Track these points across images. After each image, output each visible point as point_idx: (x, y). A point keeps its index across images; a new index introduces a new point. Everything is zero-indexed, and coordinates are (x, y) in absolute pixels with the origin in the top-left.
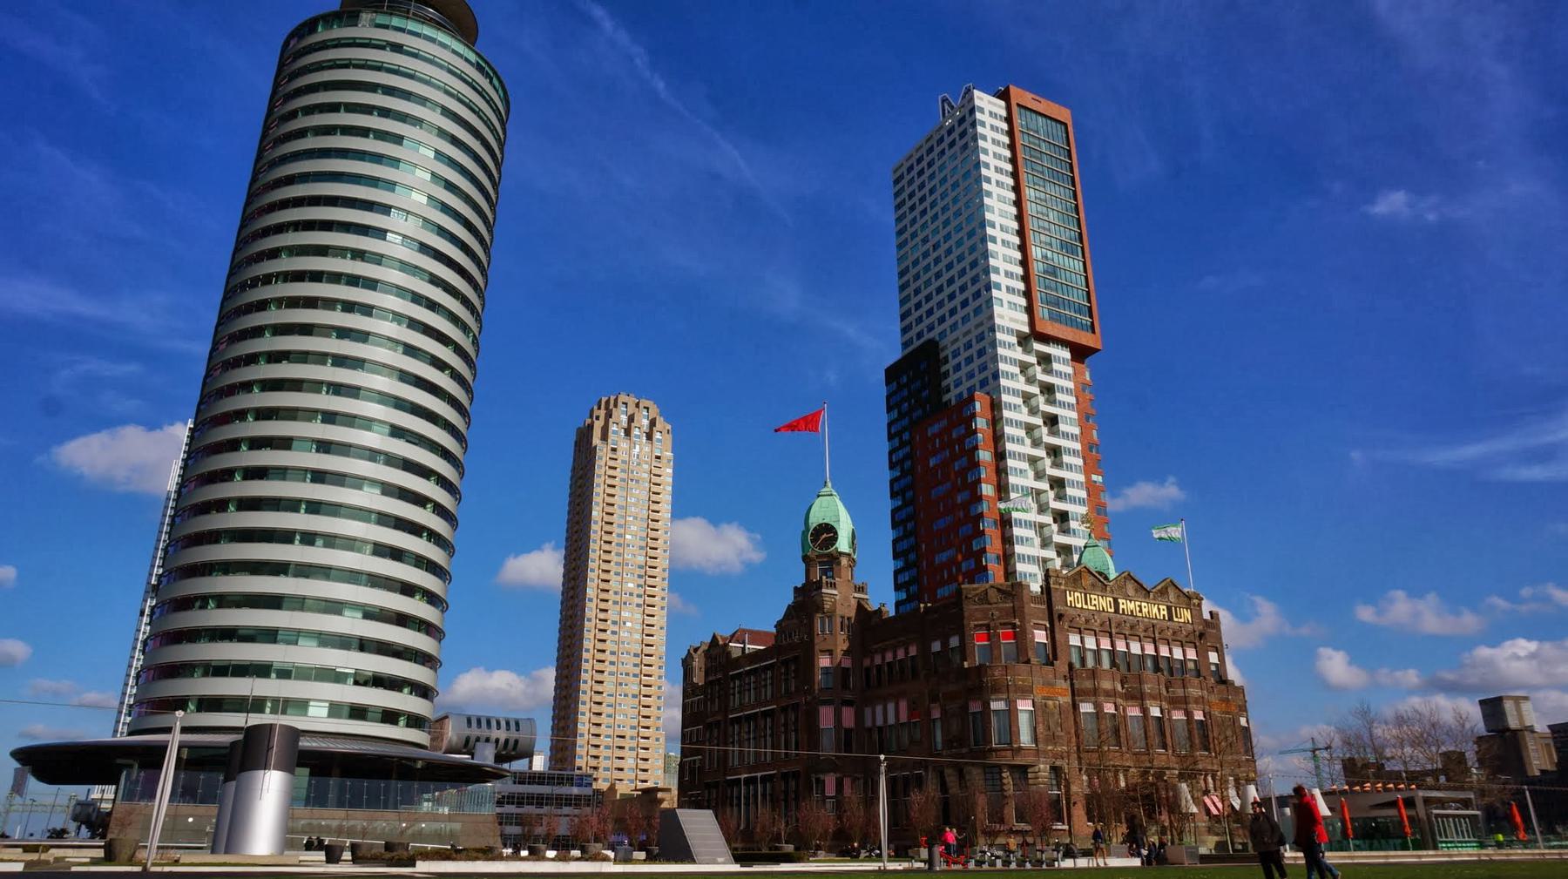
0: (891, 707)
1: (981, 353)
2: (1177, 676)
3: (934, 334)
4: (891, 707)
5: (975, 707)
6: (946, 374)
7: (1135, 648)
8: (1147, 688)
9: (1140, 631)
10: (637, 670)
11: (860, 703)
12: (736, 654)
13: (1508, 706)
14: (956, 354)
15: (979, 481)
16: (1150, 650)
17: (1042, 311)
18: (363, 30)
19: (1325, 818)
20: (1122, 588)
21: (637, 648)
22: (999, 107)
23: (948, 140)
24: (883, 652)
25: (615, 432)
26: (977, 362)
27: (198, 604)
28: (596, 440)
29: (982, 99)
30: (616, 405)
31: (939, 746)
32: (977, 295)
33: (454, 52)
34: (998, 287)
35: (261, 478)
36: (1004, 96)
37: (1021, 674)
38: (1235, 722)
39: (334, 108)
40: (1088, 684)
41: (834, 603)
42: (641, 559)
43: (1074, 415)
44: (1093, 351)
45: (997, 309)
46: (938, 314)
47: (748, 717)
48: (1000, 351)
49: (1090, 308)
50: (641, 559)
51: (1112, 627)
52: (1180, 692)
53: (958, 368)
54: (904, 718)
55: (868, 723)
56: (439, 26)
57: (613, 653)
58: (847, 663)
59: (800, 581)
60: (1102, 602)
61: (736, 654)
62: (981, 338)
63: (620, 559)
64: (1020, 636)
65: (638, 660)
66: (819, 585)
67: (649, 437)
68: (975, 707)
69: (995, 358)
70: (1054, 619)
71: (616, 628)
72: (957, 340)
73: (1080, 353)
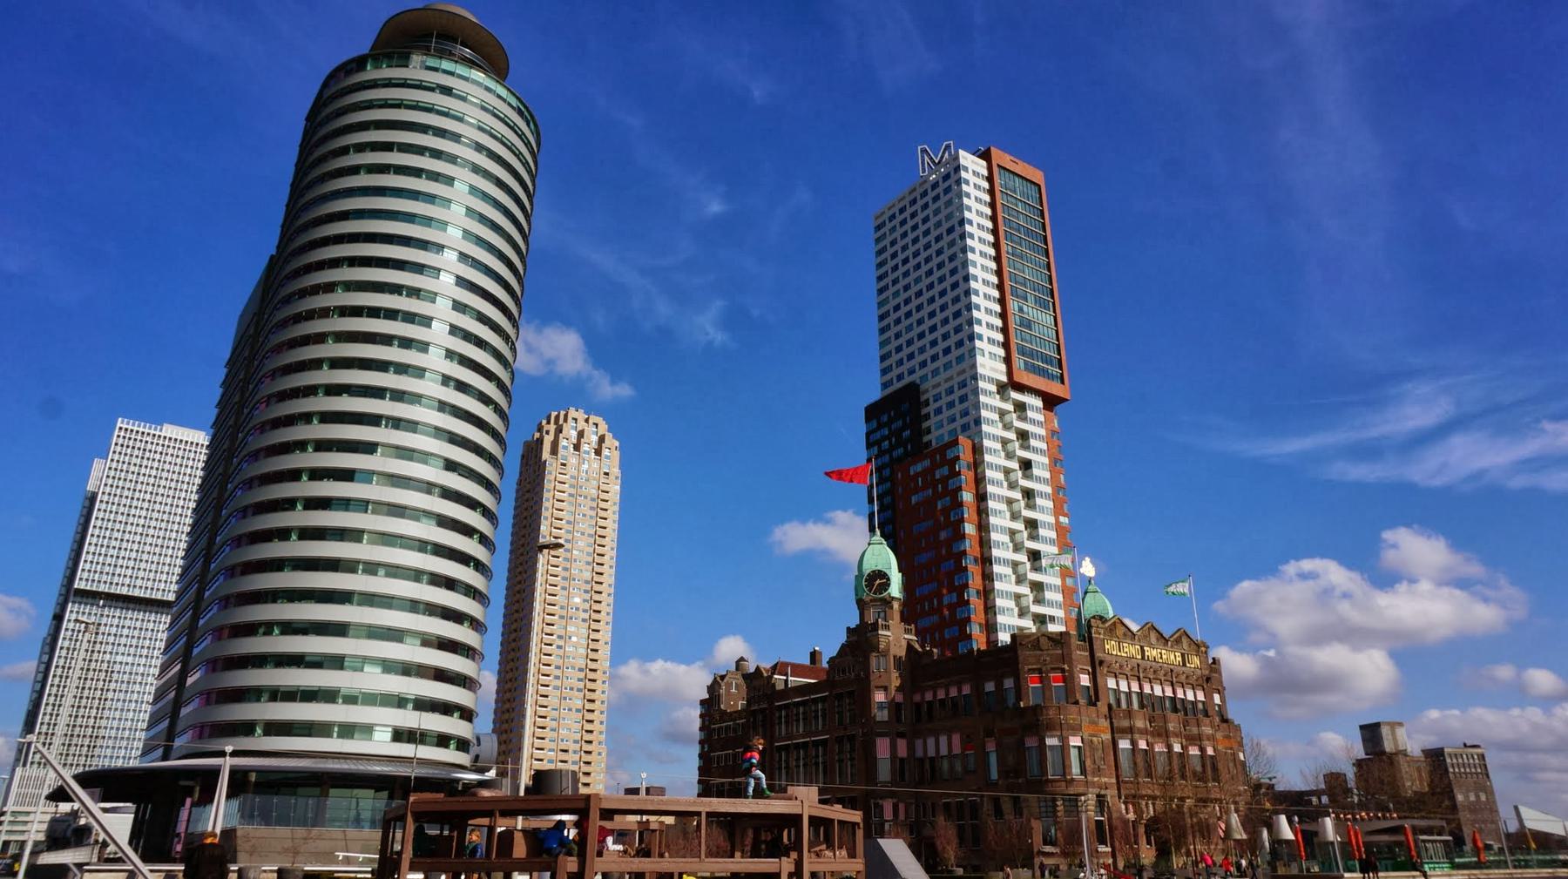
0: (943, 740)
1: (963, 399)
2: (1190, 716)
3: (915, 377)
4: (943, 740)
5: (1031, 742)
6: (927, 417)
7: (1158, 691)
8: (1171, 726)
9: (1161, 675)
10: (581, 685)
11: (912, 735)
12: (780, 686)
13: (1385, 731)
14: (937, 398)
15: (962, 520)
16: (1169, 693)
17: (1018, 361)
18: (416, 69)
19: (1288, 842)
20: (1146, 637)
21: (581, 663)
22: (981, 166)
23: (931, 194)
24: (934, 689)
25: (565, 448)
26: (959, 408)
27: (261, 630)
28: (546, 455)
29: (968, 160)
30: (566, 420)
31: (994, 775)
32: (960, 344)
33: (499, 97)
34: (980, 337)
35: (324, 508)
36: (986, 156)
37: (1071, 715)
38: (1235, 755)
39: (388, 147)
40: (1125, 723)
41: (888, 644)
42: (587, 575)
43: (1046, 460)
44: (1062, 400)
45: (979, 359)
46: (919, 358)
47: (797, 746)
48: (982, 398)
49: (1060, 361)
50: (587, 575)
51: (1139, 672)
52: (1195, 730)
53: (939, 411)
54: (957, 750)
55: (919, 754)
56: (471, 64)
57: (558, 667)
58: (899, 698)
59: (854, 622)
60: (1131, 650)
61: (780, 686)
62: (963, 385)
63: (567, 574)
64: (1069, 680)
65: (582, 675)
66: (875, 627)
67: (598, 452)
68: (1031, 742)
69: (977, 406)
70: (1095, 665)
71: (561, 643)
72: (939, 385)
73: (1051, 402)
